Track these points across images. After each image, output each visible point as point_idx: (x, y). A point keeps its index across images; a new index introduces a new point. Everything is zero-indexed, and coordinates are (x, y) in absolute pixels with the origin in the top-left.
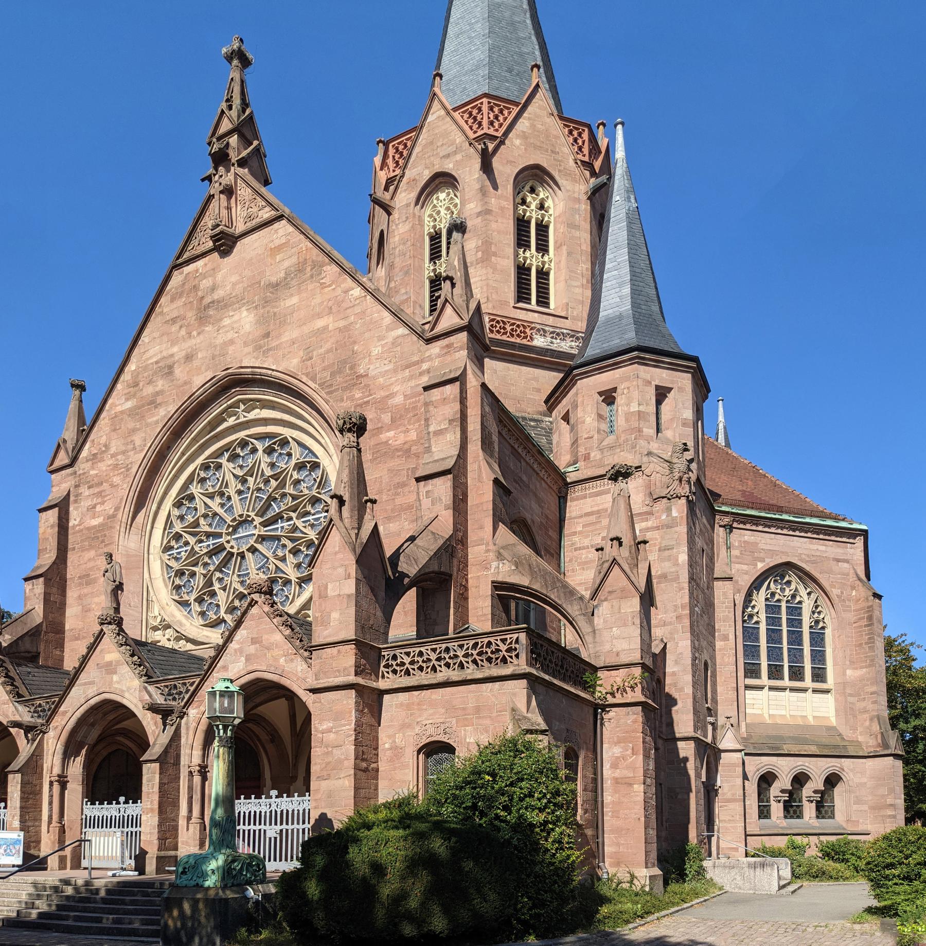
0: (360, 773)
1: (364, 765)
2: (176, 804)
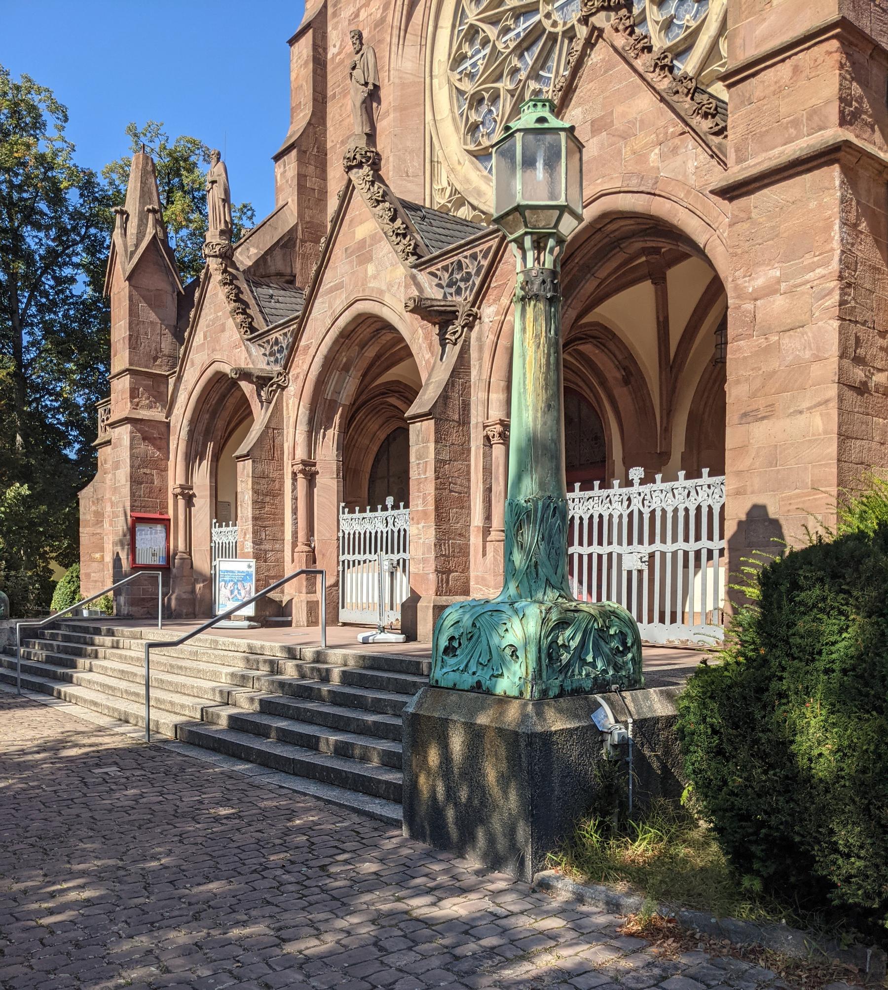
0: (850, 394)
1: (859, 374)
2: (463, 502)
